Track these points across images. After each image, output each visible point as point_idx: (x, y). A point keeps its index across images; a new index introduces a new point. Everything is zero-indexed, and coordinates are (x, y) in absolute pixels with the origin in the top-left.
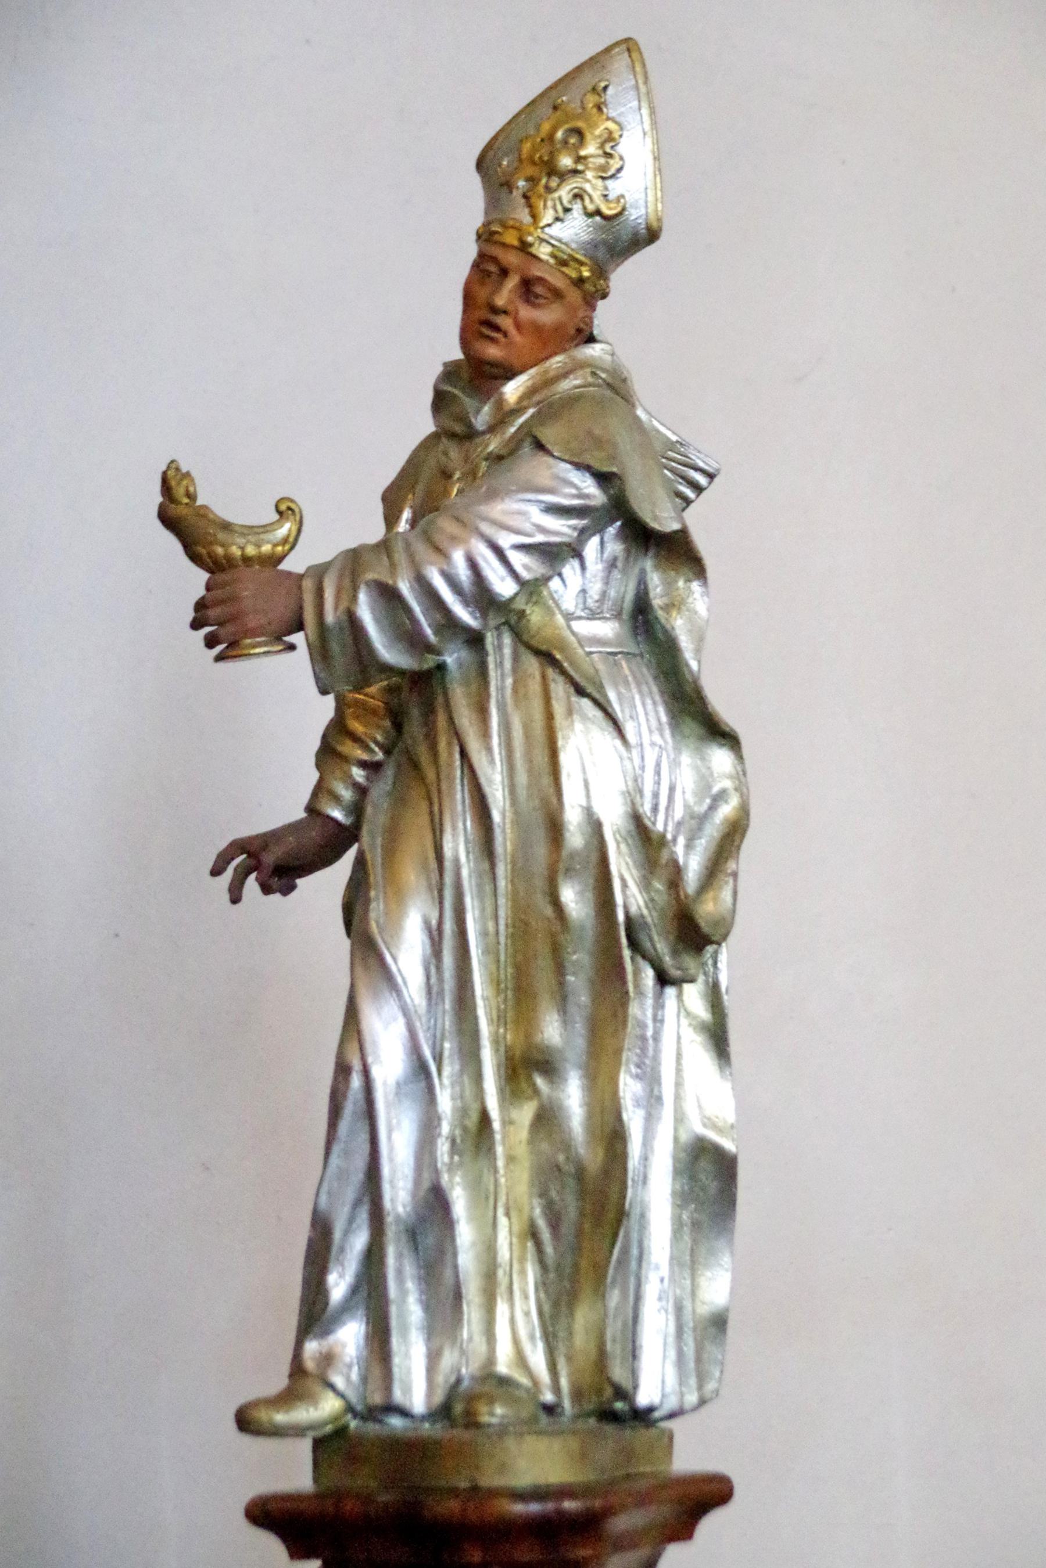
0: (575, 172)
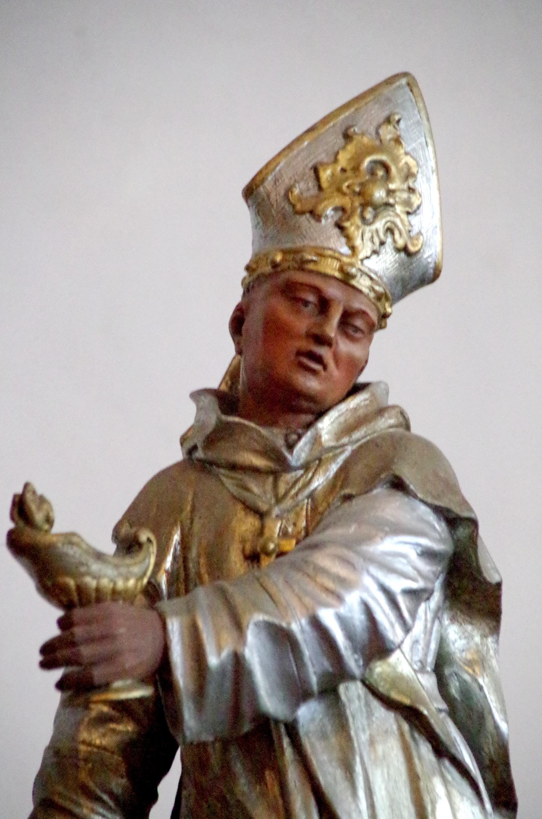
0: (387, 205)
